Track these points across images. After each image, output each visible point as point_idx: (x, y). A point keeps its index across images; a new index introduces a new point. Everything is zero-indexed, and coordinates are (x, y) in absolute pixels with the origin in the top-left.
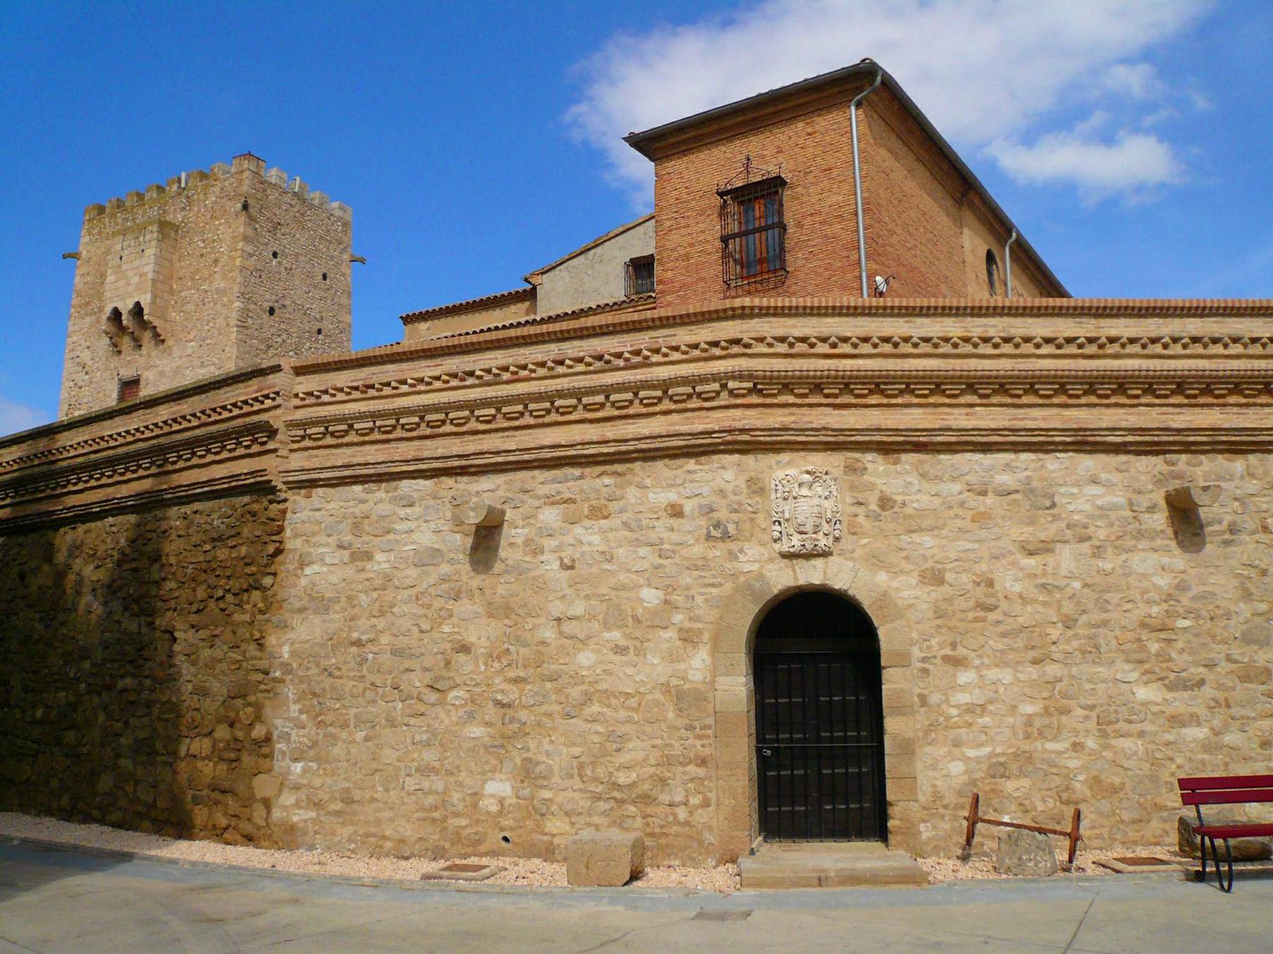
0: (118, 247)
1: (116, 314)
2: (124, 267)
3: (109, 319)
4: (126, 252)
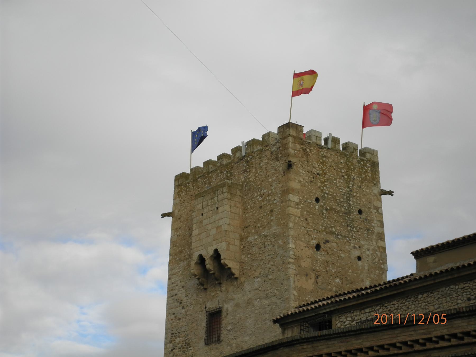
0: (199, 206)
1: (202, 260)
2: (205, 222)
3: (196, 263)
4: (205, 210)
